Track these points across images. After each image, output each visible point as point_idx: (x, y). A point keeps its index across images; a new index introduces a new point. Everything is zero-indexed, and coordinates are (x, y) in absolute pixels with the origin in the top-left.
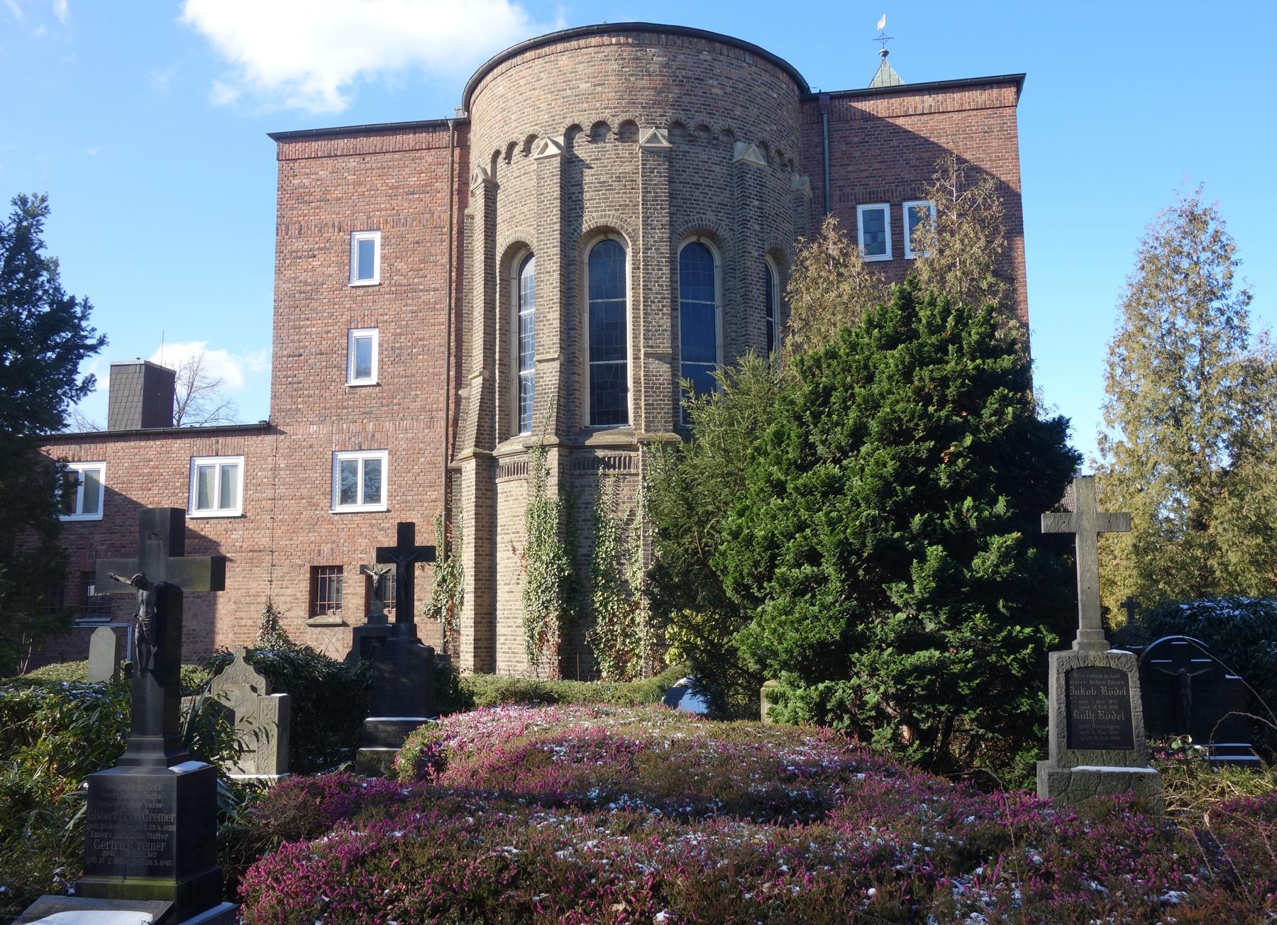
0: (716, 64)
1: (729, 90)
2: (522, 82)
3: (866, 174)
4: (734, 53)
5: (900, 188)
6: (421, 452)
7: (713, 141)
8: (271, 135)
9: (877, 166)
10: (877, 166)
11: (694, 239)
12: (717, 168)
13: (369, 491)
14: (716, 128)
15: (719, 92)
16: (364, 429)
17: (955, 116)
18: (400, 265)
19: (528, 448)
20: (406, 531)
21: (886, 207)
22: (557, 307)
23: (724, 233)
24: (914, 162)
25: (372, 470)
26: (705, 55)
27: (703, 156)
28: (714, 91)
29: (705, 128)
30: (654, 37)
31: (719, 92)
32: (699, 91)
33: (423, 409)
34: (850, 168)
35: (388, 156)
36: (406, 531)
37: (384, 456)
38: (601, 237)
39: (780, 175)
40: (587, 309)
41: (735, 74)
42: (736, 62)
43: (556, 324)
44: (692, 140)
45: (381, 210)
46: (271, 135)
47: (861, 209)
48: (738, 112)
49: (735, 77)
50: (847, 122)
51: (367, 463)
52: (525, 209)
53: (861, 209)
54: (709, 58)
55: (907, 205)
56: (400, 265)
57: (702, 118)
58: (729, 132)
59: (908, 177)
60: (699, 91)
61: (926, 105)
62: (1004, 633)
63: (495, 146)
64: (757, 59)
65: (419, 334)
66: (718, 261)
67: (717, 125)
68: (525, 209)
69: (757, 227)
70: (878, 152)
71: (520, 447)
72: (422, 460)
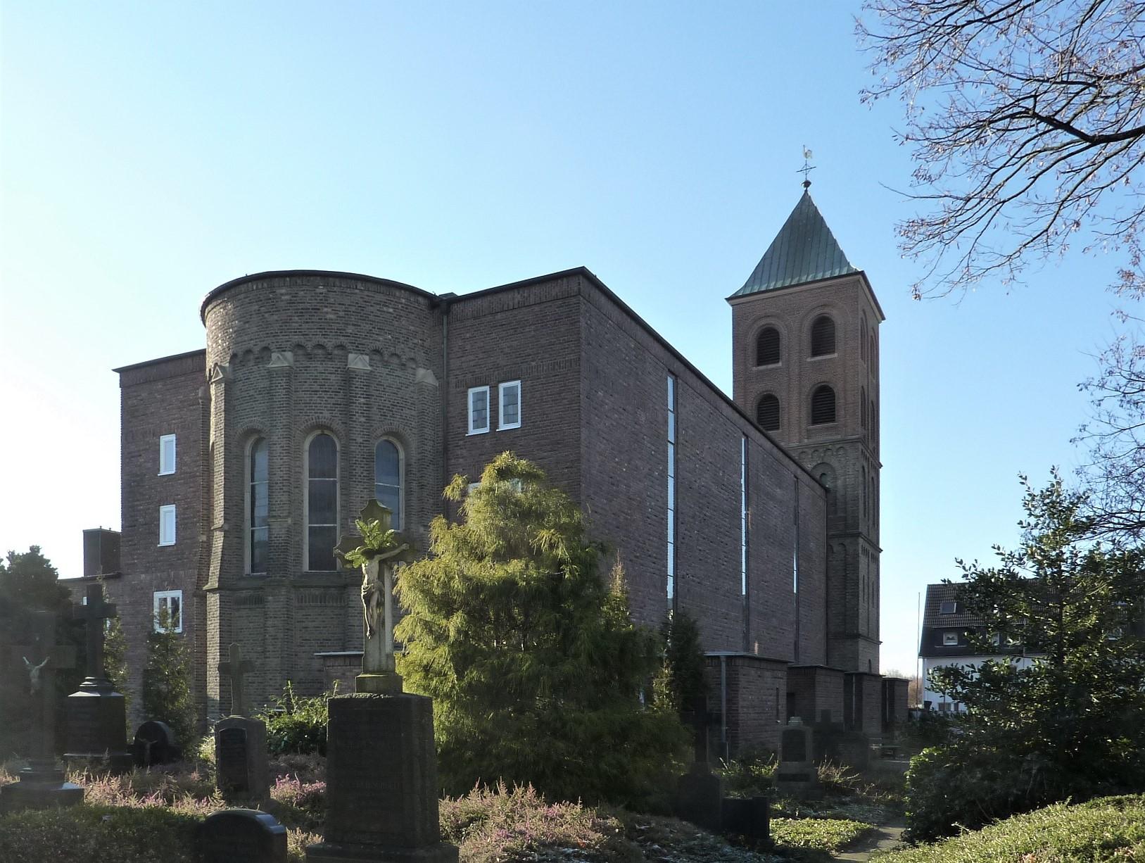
0: (331, 295)
1: (341, 314)
7: (329, 356)
9: (481, 356)
10: (481, 356)
12: (333, 377)
13: (226, 628)
14: (309, 345)
17: (537, 308)
18: (186, 459)
21: (487, 388)
24: (507, 350)
26: (321, 289)
27: (321, 369)
28: (329, 316)
32: (315, 319)
38: (319, 432)
39: (399, 373)
40: (306, 485)
44: (309, 356)
48: (350, 330)
51: (173, 599)
55: (502, 386)
56: (186, 459)
57: (316, 340)
64: (369, 285)
67: (330, 343)
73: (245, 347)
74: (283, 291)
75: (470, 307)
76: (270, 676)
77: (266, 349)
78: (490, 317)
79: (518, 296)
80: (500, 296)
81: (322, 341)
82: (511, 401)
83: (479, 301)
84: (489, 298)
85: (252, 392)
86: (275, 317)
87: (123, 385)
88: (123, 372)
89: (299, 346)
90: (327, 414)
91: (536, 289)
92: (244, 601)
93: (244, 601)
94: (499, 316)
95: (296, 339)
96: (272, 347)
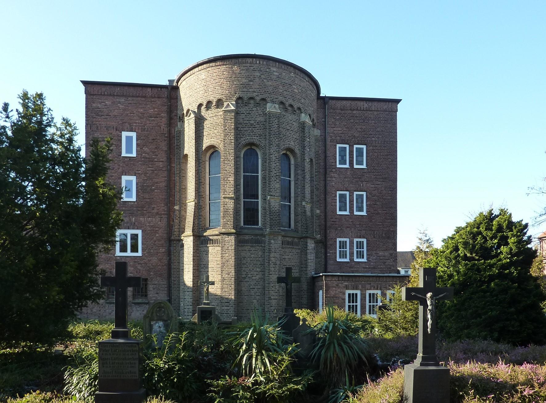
2: (214, 74)
3: (341, 132)
4: (302, 75)
5: (353, 139)
6: (156, 232)
8: (82, 81)
9: (345, 129)
10: (345, 129)
11: (284, 152)
12: (295, 123)
14: (287, 104)
15: (297, 91)
16: (130, 220)
17: (375, 113)
18: (145, 149)
19: (221, 234)
20: (289, 270)
22: (233, 176)
23: (297, 151)
25: (134, 237)
28: (295, 90)
29: (291, 106)
30: (274, 64)
31: (297, 91)
33: (157, 213)
34: (335, 129)
35: (139, 99)
36: (289, 270)
37: (139, 232)
40: (242, 177)
41: (302, 84)
42: (302, 79)
43: (232, 182)
44: (286, 110)
45: (136, 123)
46: (82, 81)
47: (338, 146)
49: (302, 85)
50: (334, 110)
52: (216, 132)
53: (338, 146)
54: (293, 76)
57: (291, 101)
58: (299, 109)
59: (357, 135)
60: (290, 90)
61: (365, 107)
62: (428, 311)
63: (200, 102)
65: (156, 180)
66: (292, 162)
68: (216, 132)
69: (308, 150)
70: (345, 124)
71: (217, 233)
72: (157, 235)
73: (250, 95)
74: (275, 70)
75: (339, 104)
76: (272, 285)
77: (263, 99)
78: (350, 111)
79: (366, 105)
80: (356, 102)
81: (293, 103)
82: (343, 157)
83: (345, 102)
84: (350, 102)
85: (252, 122)
86: (270, 83)
87: (86, 92)
88: (90, 86)
89: (282, 103)
90: (292, 143)
91: (108, 87)
92: (288, 243)
93: (288, 243)
94: (355, 112)
95: (281, 98)
96: (268, 100)
